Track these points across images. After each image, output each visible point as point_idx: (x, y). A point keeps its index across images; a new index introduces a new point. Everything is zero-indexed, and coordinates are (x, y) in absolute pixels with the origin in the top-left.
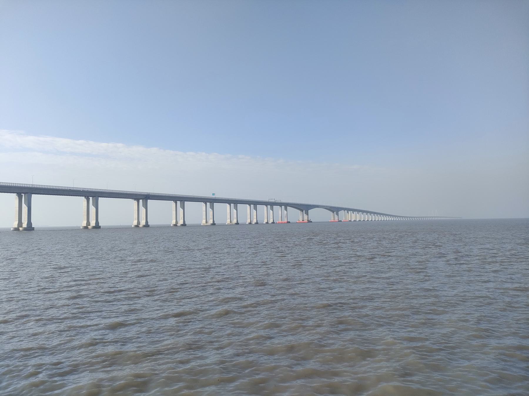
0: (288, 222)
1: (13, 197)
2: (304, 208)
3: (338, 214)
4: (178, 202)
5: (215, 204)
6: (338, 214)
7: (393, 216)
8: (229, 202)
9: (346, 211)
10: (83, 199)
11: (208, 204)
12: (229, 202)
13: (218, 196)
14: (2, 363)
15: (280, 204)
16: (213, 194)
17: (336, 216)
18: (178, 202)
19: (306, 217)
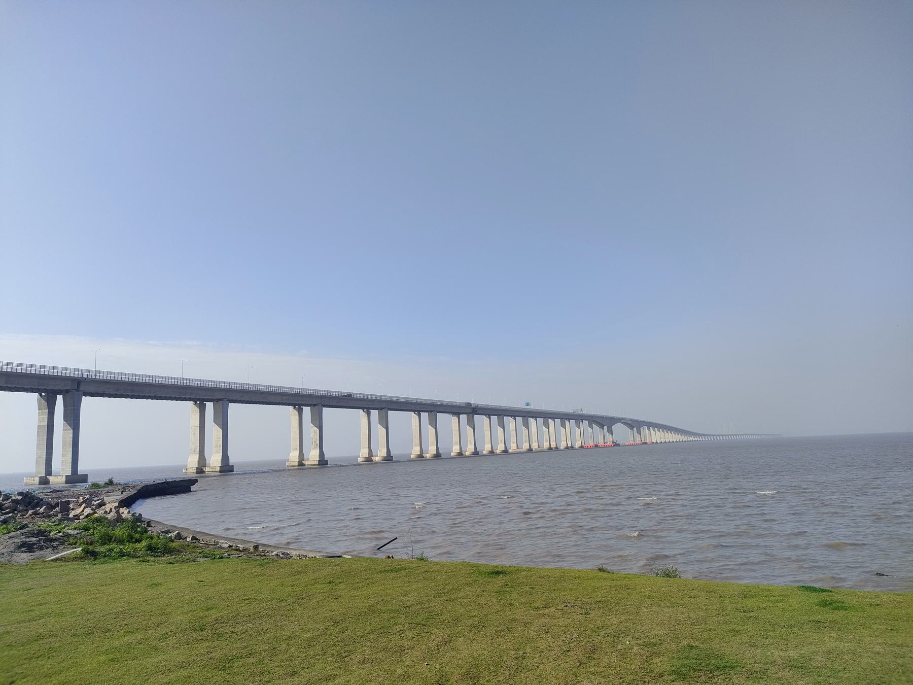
0: (596, 446)
1: (28, 403)
2: (604, 422)
3: (610, 431)
4: (209, 406)
5: (234, 409)
6: (610, 431)
7: (700, 435)
8: (366, 404)
9: (463, 417)
10: (189, 407)
11: (307, 410)
12: (366, 404)
13: (534, 406)
14: (910, 575)
15: (455, 410)
16: (528, 404)
17: (637, 435)
18: (209, 406)
19: (609, 438)
